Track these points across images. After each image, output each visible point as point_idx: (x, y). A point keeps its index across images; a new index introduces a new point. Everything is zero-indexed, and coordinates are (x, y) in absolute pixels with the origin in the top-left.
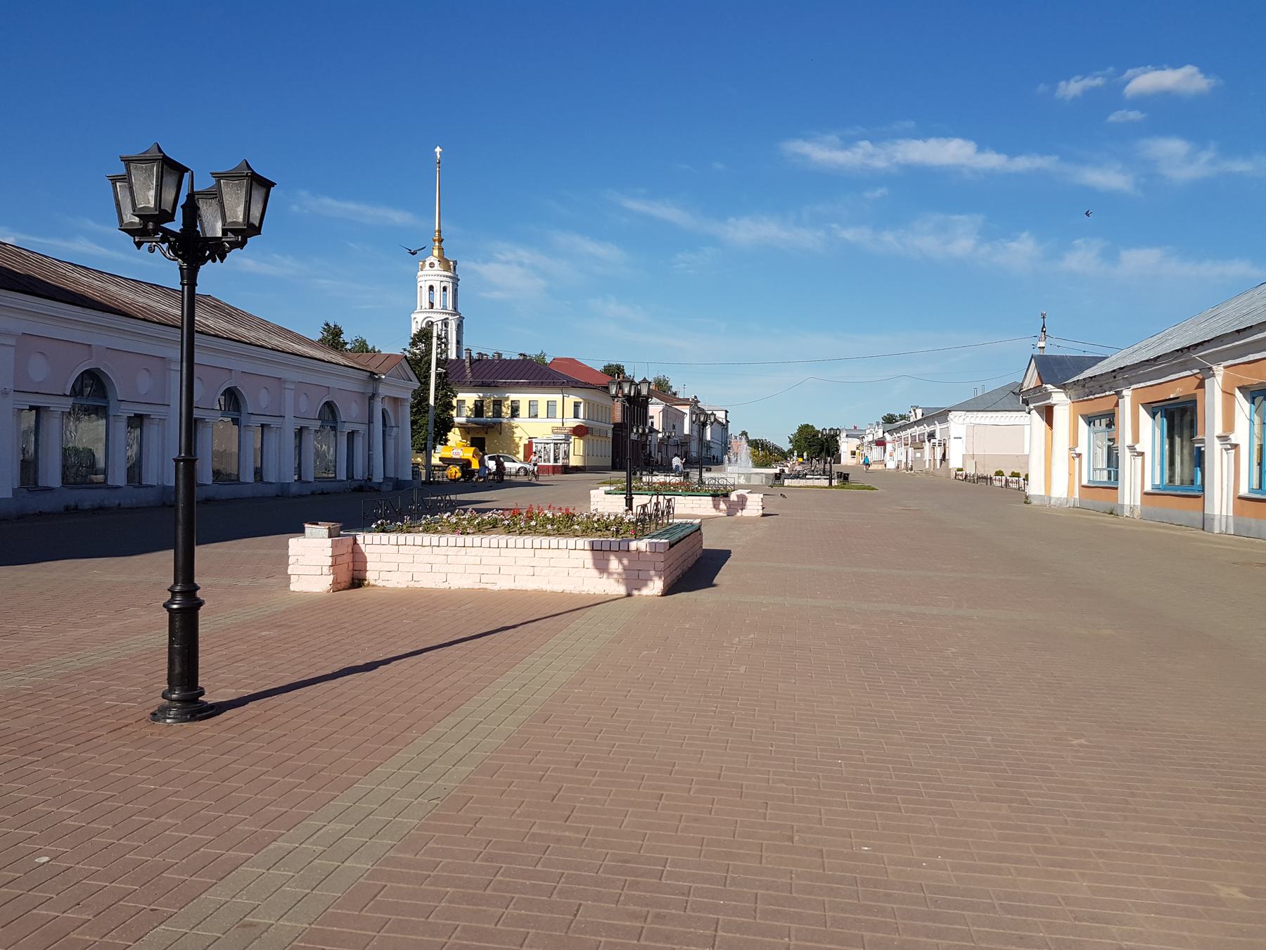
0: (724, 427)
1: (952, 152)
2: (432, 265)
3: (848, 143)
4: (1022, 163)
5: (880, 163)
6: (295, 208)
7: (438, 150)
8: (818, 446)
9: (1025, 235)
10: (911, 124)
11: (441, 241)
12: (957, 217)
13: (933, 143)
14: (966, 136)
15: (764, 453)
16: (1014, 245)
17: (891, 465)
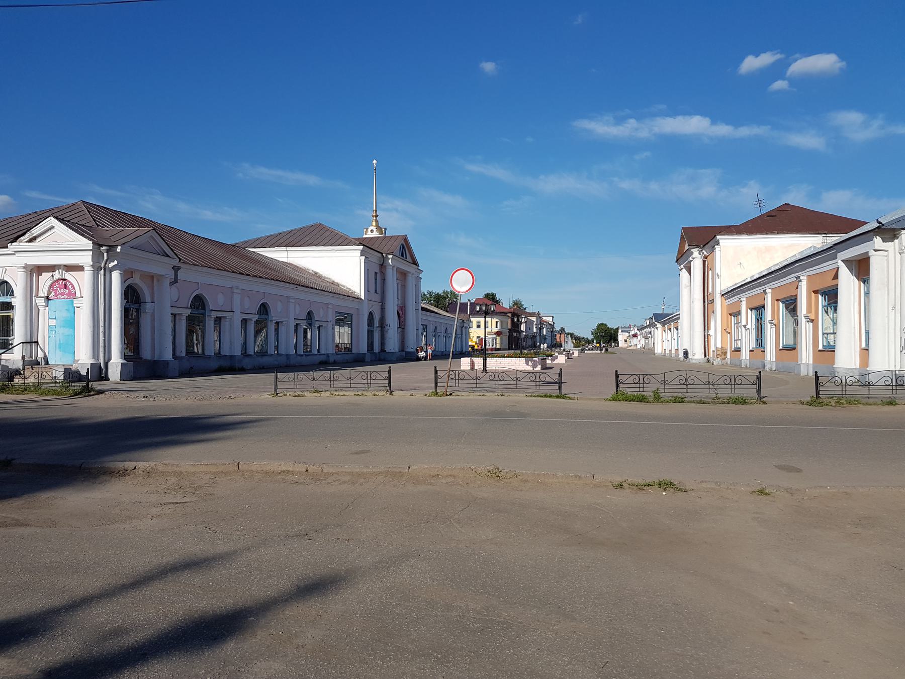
0: (552, 326)
1: (695, 125)
2: (372, 231)
3: (620, 121)
4: (744, 131)
5: (644, 134)
6: (241, 175)
7: (375, 162)
8: (606, 336)
9: (752, 183)
10: (663, 107)
11: (377, 216)
12: (703, 171)
13: (680, 118)
14: (703, 114)
15: (580, 342)
16: (744, 190)
17: (639, 347)
